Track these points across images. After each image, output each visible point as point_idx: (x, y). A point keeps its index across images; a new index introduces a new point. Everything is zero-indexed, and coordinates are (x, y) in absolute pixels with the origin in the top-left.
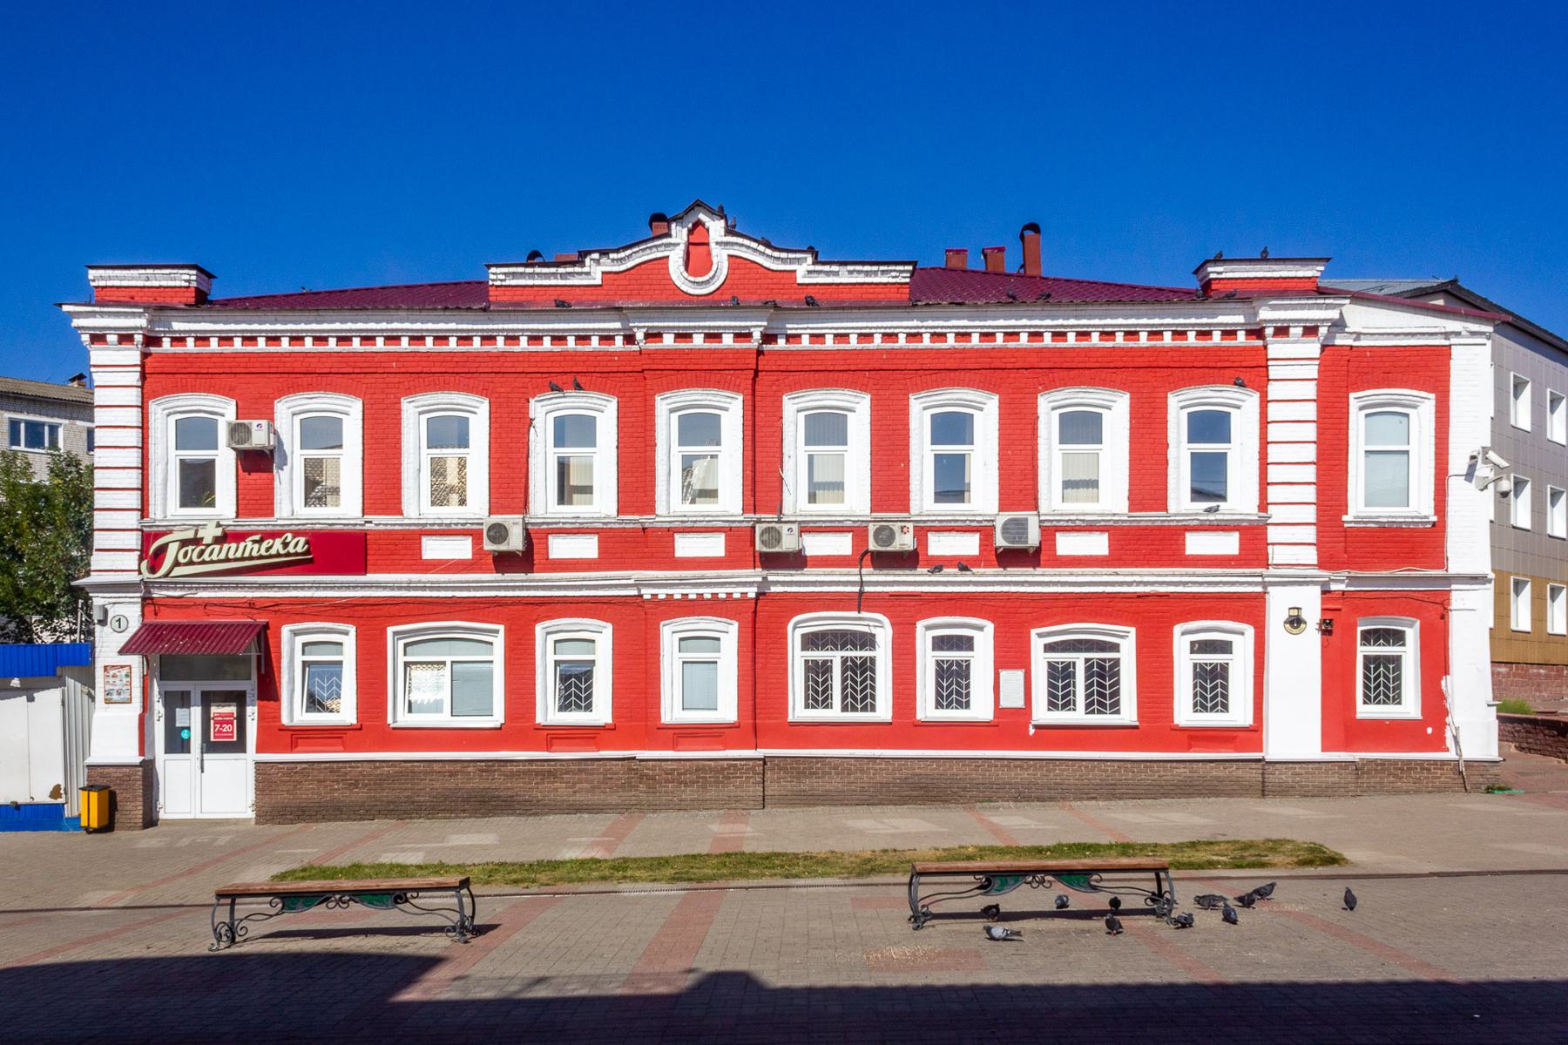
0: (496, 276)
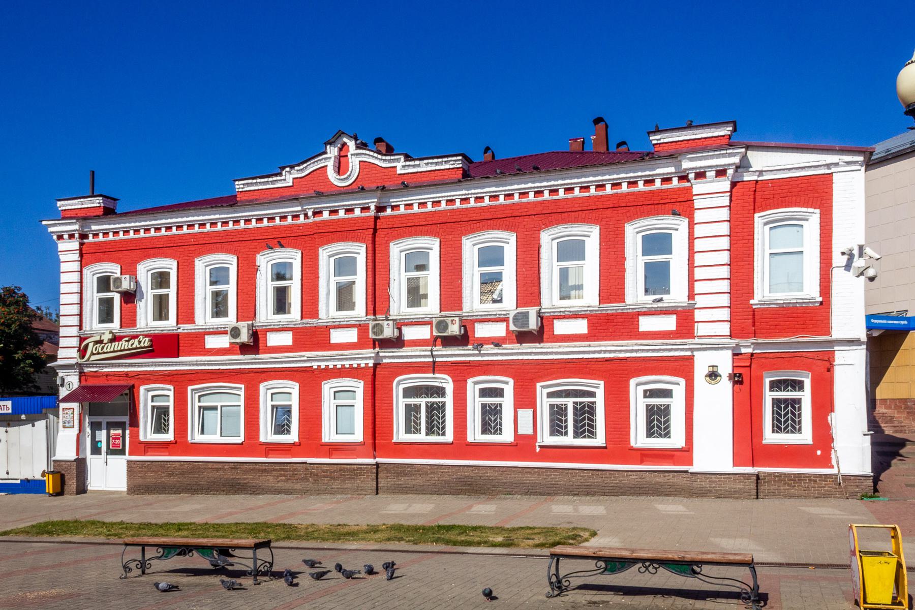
0: (239, 186)
